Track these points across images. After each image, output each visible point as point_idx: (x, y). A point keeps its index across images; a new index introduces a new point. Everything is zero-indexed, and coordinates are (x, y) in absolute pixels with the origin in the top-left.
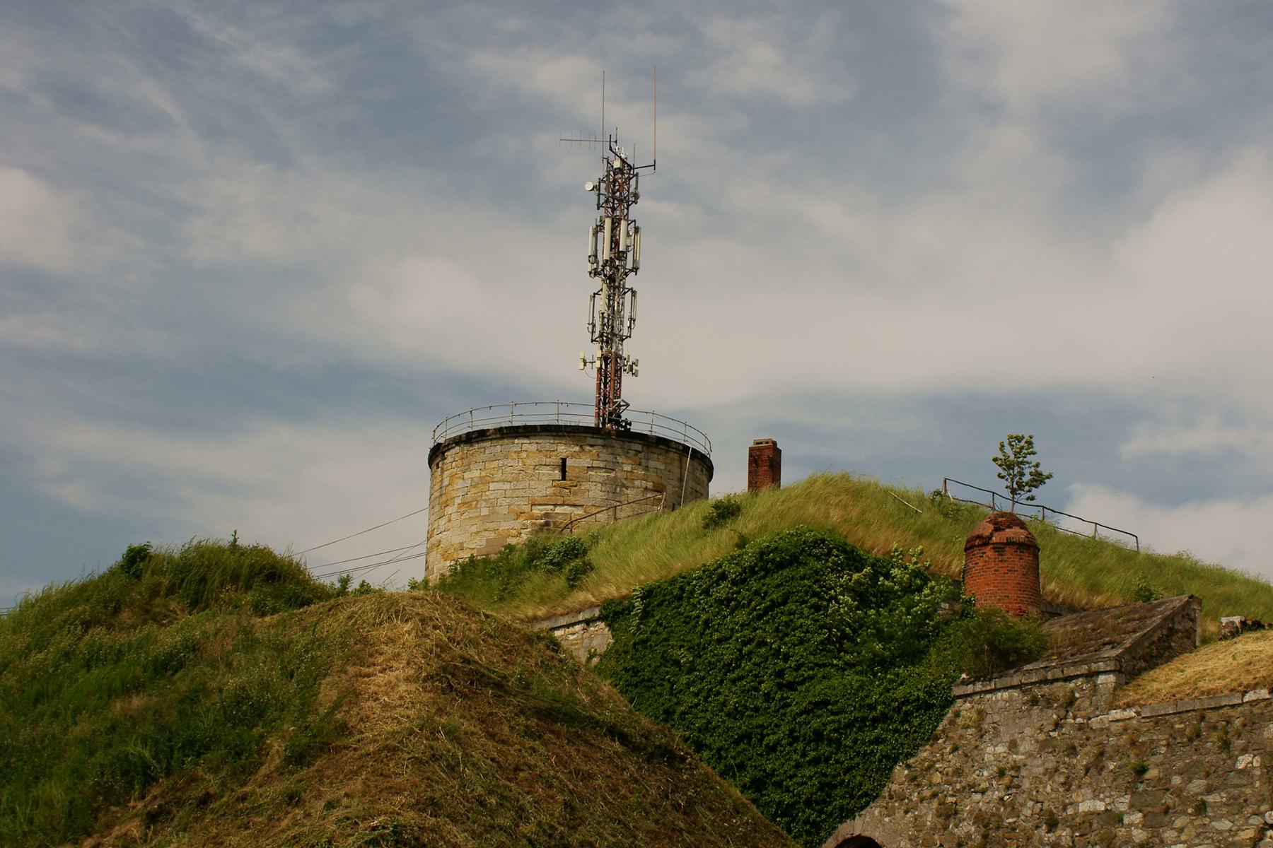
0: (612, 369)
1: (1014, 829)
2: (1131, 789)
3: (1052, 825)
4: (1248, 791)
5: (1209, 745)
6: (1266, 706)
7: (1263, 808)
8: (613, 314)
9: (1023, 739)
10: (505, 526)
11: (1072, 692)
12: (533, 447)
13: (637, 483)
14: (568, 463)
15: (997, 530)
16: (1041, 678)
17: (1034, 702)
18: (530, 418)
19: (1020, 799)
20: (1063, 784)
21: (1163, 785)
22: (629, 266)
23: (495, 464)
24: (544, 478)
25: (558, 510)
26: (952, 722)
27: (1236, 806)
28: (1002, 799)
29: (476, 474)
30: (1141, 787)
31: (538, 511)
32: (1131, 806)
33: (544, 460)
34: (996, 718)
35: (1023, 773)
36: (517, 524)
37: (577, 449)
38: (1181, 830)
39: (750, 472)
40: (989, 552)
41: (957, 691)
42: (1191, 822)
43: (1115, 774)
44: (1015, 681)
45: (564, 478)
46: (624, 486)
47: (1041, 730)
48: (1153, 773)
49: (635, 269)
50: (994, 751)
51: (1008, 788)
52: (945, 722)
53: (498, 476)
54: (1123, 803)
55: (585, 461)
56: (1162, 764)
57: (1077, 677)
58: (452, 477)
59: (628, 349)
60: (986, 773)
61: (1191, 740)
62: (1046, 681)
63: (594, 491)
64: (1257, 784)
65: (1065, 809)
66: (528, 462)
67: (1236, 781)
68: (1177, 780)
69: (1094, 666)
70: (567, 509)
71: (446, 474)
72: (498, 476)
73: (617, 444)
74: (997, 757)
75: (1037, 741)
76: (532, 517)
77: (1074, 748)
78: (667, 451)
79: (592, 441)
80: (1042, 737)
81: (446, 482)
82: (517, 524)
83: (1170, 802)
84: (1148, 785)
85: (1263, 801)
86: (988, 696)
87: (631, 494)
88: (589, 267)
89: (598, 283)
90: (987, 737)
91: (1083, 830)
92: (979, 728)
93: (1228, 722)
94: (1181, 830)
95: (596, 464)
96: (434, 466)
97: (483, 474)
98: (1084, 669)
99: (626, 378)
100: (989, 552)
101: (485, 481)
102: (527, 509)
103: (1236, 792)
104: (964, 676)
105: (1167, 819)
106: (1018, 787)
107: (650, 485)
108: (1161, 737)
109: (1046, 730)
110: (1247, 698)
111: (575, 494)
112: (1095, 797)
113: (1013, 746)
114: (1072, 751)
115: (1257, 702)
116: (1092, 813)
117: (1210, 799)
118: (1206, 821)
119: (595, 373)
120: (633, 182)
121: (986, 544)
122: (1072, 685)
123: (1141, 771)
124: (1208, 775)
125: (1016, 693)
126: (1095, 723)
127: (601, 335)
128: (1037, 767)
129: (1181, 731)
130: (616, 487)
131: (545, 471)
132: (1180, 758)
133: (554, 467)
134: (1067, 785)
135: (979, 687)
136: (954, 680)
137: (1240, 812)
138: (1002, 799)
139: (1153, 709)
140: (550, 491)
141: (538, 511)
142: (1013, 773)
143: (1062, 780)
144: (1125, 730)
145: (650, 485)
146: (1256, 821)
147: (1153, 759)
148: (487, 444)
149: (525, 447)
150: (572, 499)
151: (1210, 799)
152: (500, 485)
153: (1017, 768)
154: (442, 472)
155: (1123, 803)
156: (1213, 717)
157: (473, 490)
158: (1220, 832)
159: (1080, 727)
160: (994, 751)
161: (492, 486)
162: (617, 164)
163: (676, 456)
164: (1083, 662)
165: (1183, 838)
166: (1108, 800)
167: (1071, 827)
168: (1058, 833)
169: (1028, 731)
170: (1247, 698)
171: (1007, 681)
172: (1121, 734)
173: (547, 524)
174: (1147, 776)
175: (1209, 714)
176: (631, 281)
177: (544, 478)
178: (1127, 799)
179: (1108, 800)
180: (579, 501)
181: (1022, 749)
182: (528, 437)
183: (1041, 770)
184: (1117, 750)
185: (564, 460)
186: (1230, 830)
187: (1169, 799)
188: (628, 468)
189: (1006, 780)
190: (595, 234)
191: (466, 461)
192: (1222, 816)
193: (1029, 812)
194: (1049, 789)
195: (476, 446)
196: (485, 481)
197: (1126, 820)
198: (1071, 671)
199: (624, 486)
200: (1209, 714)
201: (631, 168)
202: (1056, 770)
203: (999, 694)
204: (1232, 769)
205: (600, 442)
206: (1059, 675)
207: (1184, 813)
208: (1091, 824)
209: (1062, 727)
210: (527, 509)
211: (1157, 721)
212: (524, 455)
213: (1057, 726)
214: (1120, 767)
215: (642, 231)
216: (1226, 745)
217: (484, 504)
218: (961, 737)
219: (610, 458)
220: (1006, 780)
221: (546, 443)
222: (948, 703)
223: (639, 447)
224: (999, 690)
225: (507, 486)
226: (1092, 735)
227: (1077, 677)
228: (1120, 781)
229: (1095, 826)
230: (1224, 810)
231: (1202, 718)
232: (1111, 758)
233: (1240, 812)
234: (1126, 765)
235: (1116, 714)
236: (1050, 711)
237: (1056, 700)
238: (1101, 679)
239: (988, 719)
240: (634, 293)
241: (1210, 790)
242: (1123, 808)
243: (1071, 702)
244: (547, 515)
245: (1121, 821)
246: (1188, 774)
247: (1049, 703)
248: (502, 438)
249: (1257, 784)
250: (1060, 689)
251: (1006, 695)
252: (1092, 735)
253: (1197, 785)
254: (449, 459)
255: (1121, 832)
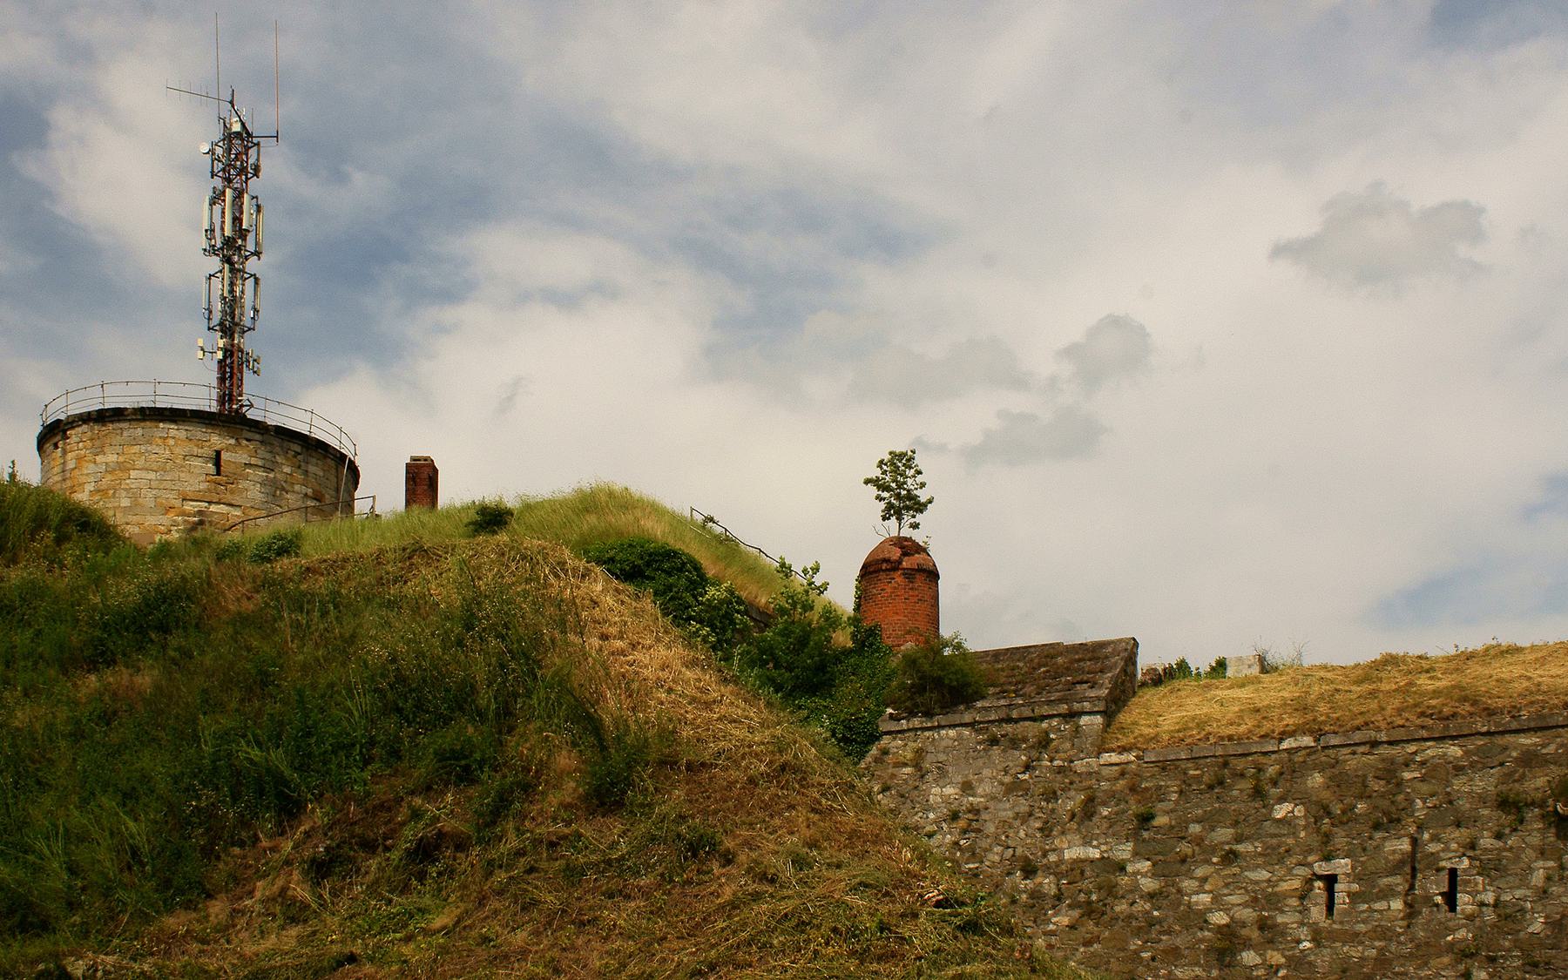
0: (231, 367)
1: (976, 875)
2: (1134, 835)
3: (1029, 871)
4: (1290, 841)
5: (1235, 793)
6: (1309, 755)
7: (1310, 859)
8: (232, 303)
9: (981, 781)
10: (151, 520)
11: (1047, 734)
12: (182, 434)
13: (297, 487)
14: (224, 456)
15: (905, 554)
16: (1003, 715)
17: (994, 741)
18: (175, 400)
19: (984, 844)
20: (1041, 829)
21: (1178, 832)
22: (251, 247)
23: (136, 449)
24: (197, 471)
25: (213, 508)
26: (877, 760)
27: (1275, 856)
28: (957, 843)
29: (112, 458)
30: (1146, 835)
31: (190, 507)
32: (1136, 854)
33: (196, 451)
34: (942, 757)
35: (984, 816)
36: (166, 520)
37: (232, 441)
38: (1204, 880)
39: (407, 490)
40: (898, 578)
41: (883, 727)
42: (1217, 872)
43: (1111, 821)
44: (967, 718)
45: (218, 473)
46: (283, 489)
47: (1006, 773)
48: (1161, 820)
49: (257, 254)
50: (943, 793)
51: (965, 831)
52: (868, 759)
53: (140, 463)
54: (1124, 851)
55: (242, 457)
56: (1172, 811)
57: (1054, 716)
58: (79, 459)
59: (247, 343)
60: (932, 816)
61: (1211, 787)
62: (1009, 720)
63: (252, 490)
64: (1303, 834)
65: (1045, 855)
66: (177, 450)
67: (1272, 831)
68: (1195, 828)
69: (1076, 706)
70: (222, 508)
71: (70, 456)
72: (140, 463)
73: (276, 442)
74: (946, 800)
75: (1002, 784)
76: (183, 514)
77: (1055, 793)
78: (325, 457)
79: (250, 435)
80: (1007, 779)
81: (71, 465)
82: (166, 520)
83: (1189, 851)
84: (1157, 833)
85: (1310, 851)
86: (927, 734)
87: (292, 499)
88: (205, 244)
89: (215, 263)
90: (929, 777)
91: (1071, 878)
92: (917, 766)
93: (1260, 770)
94: (1204, 880)
95: (254, 461)
96: (49, 447)
97: (121, 459)
98: (1064, 708)
99: (248, 376)
100: (898, 578)
101: (123, 468)
102: (177, 503)
103: (1274, 841)
104: (890, 710)
105: (1184, 868)
106: (979, 831)
107: (310, 491)
108: (1173, 786)
109: (1013, 771)
110: (1285, 745)
111: (232, 492)
112: (1086, 842)
113: (967, 788)
114: (1051, 796)
115: (1298, 749)
116: (1082, 861)
117: (1240, 848)
118: (1236, 870)
119: (215, 366)
120: (253, 152)
121: (895, 569)
122: (1044, 725)
123: (1145, 819)
124: (1236, 824)
125: (966, 732)
126: (1079, 766)
127: (221, 324)
128: (1006, 810)
129: (1197, 779)
130: (275, 490)
131: (197, 462)
132: (1198, 806)
133: (207, 459)
134: (1046, 831)
135: (916, 722)
136: (881, 713)
137: (1281, 861)
138: (957, 843)
139: (1158, 754)
140: (203, 486)
141: (190, 507)
142: (970, 816)
143: (1038, 825)
144: (1123, 774)
145: (310, 491)
146: (1303, 871)
147: (1159, 805)
148: (122, 425)
149: (173, 433)
150: (229, 497)
151: (1240, 848)
152: (144, 474)
153: (975, 810)
154: (65, 452)
155: (1124, 851)
156: (1240, 764)
157: (109, 477)
158: (1257, 883)
159: (1060, 770)
160: (943, 793)
161: (133, 474)
162: (237, 128)
163: (332, 463)
164: (1060, 701)
165: (1207, 887)
166: (1104, 848)
167: (1055, 874)
168: (1038, 880)
169: (986, 772)
170: (1285, 745)
171: (956, 718)
172: (1117, 779)
173: (201, 523)
174: (1156, 822)
175: (1233, 761)
176: (252, 265)
177: (197, 471)
178: (1129, 846)
179: (1104, 848)
180: (237, 500)
181: (980, 791)
182: (175, 422)
183: (1010, 814)
184: (1112, 795)
185: (218, 453)
186: (1269, 881)
187: (1184, 848)
188: (287, 470)
189: (962, 823)
190: (212, 203)
191: (98, 443)
192: (1258, 866)
193: (997, 858)
194: (1022, 834)
195: (111, 426)
196: (123, 468)
197: (1130, 869)
198: (1046, 710)
199: (283, 489)
200: (1233, 761)
201: (249, 135)
202: (1030, 815)
203: (943, 732)
204: (1268, 817)
205: (257, 437)
206: (1027, 712)
207: (1208, 862)
208: (1082, 873)
209: (1034, 768)
210: (177, 503)
211: (1164, 766)
212: (172, 442)
213: (1027, 768)
214: (1117, 814)
215: (264, 210)
216: (1258, 793)
217: (124, 494)
218: (893, 776)
219: (268, 456)
220: (962, 823)
221: (198, 432)
222: (874, 737)
223: (298, 449)
224: (943, 727)
225: (152, 475)
226: (1077, 780)
227: (1054, 716)
228: (1117, 828)
229: (1088, 873)
230: (1260, 861)
231: (1226, 764)
232: (1104, 804)
233: (1281, 861)
234: (1124, 812)
235: (1108, 757)
236: (1017, 753)
237: (1025, 740)
238: (1084, 720)
239: (929, 758)
240: (257, 280)
241: (1239, 839)
242: (1126, 855)
243: (1044, 743)
244: (200, 513)
245: (1122, 869)
246: (1210, 821)
247: (1014, 743)
248: (144, 420)
249: (1303, 834)
250: (1031, 730)
251: (952, 733)
252: (1077, 780)
253: (1224, 834)
254: (74, 439)
255: (1124, 880)
